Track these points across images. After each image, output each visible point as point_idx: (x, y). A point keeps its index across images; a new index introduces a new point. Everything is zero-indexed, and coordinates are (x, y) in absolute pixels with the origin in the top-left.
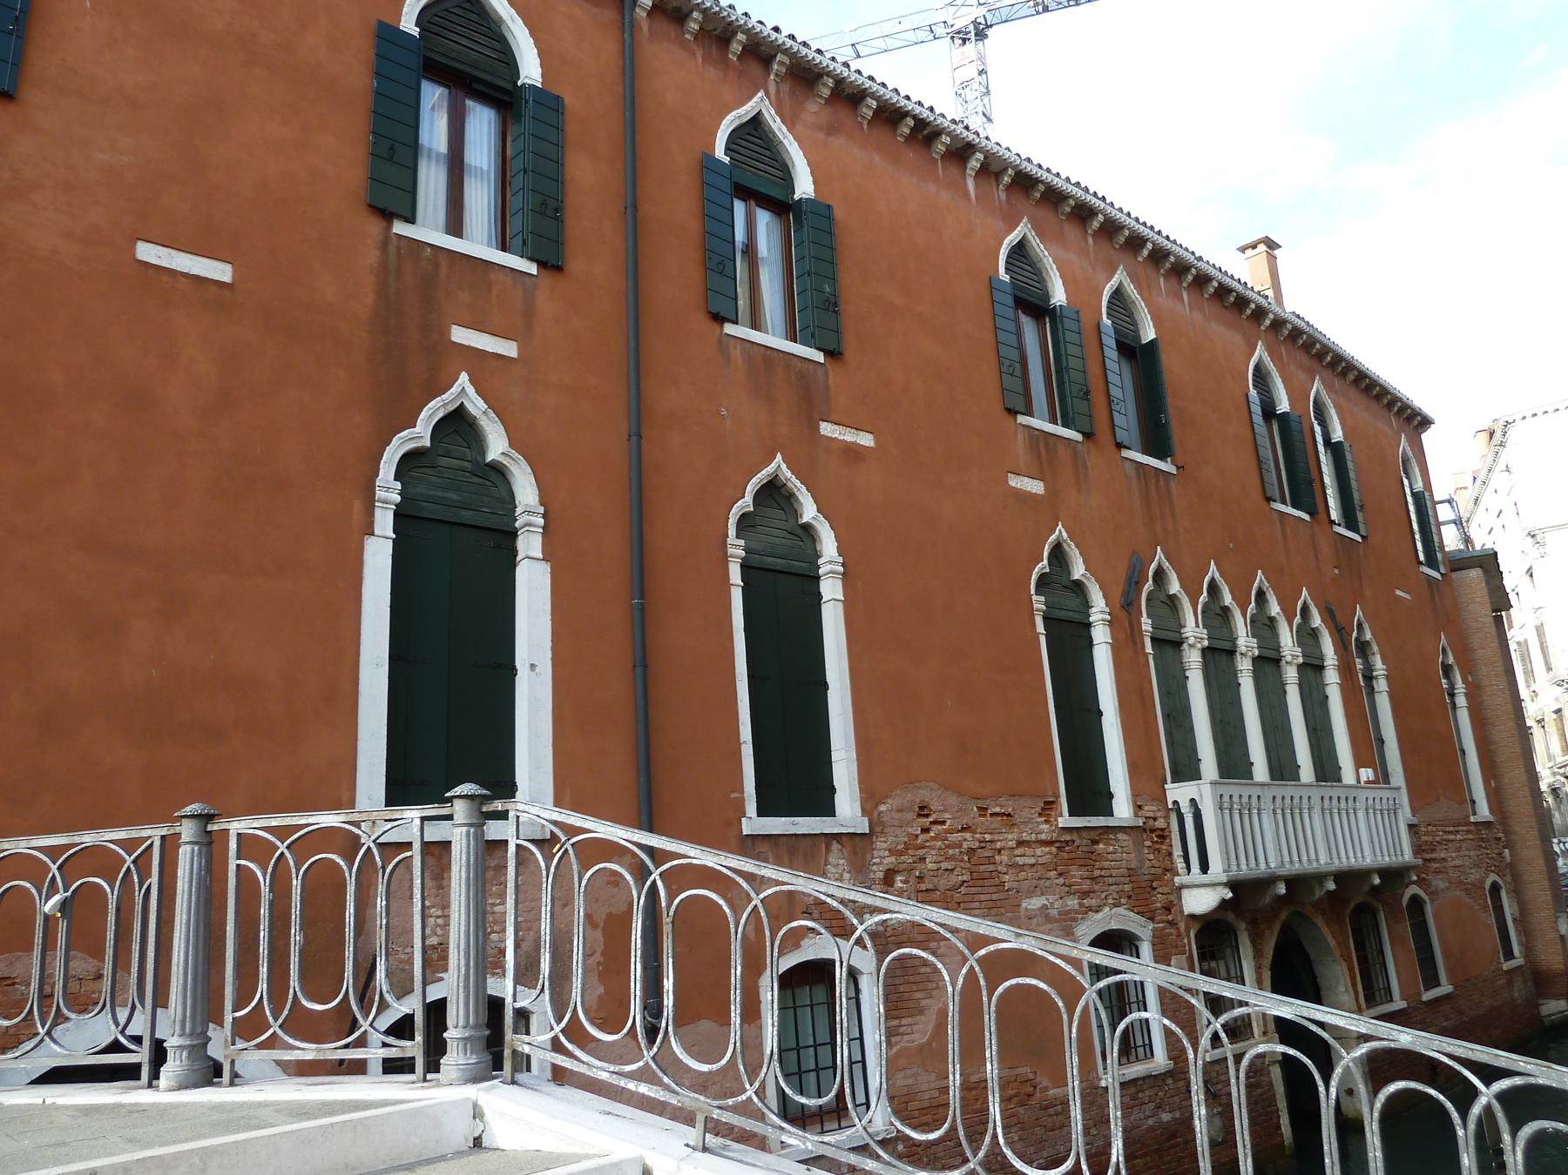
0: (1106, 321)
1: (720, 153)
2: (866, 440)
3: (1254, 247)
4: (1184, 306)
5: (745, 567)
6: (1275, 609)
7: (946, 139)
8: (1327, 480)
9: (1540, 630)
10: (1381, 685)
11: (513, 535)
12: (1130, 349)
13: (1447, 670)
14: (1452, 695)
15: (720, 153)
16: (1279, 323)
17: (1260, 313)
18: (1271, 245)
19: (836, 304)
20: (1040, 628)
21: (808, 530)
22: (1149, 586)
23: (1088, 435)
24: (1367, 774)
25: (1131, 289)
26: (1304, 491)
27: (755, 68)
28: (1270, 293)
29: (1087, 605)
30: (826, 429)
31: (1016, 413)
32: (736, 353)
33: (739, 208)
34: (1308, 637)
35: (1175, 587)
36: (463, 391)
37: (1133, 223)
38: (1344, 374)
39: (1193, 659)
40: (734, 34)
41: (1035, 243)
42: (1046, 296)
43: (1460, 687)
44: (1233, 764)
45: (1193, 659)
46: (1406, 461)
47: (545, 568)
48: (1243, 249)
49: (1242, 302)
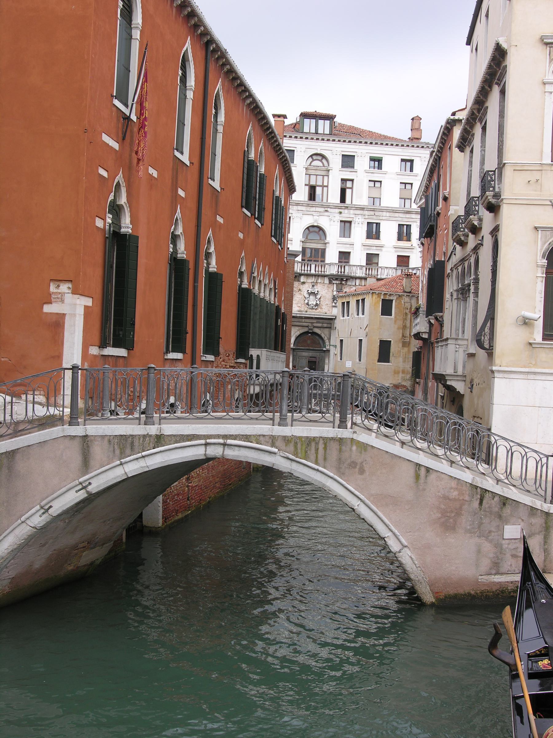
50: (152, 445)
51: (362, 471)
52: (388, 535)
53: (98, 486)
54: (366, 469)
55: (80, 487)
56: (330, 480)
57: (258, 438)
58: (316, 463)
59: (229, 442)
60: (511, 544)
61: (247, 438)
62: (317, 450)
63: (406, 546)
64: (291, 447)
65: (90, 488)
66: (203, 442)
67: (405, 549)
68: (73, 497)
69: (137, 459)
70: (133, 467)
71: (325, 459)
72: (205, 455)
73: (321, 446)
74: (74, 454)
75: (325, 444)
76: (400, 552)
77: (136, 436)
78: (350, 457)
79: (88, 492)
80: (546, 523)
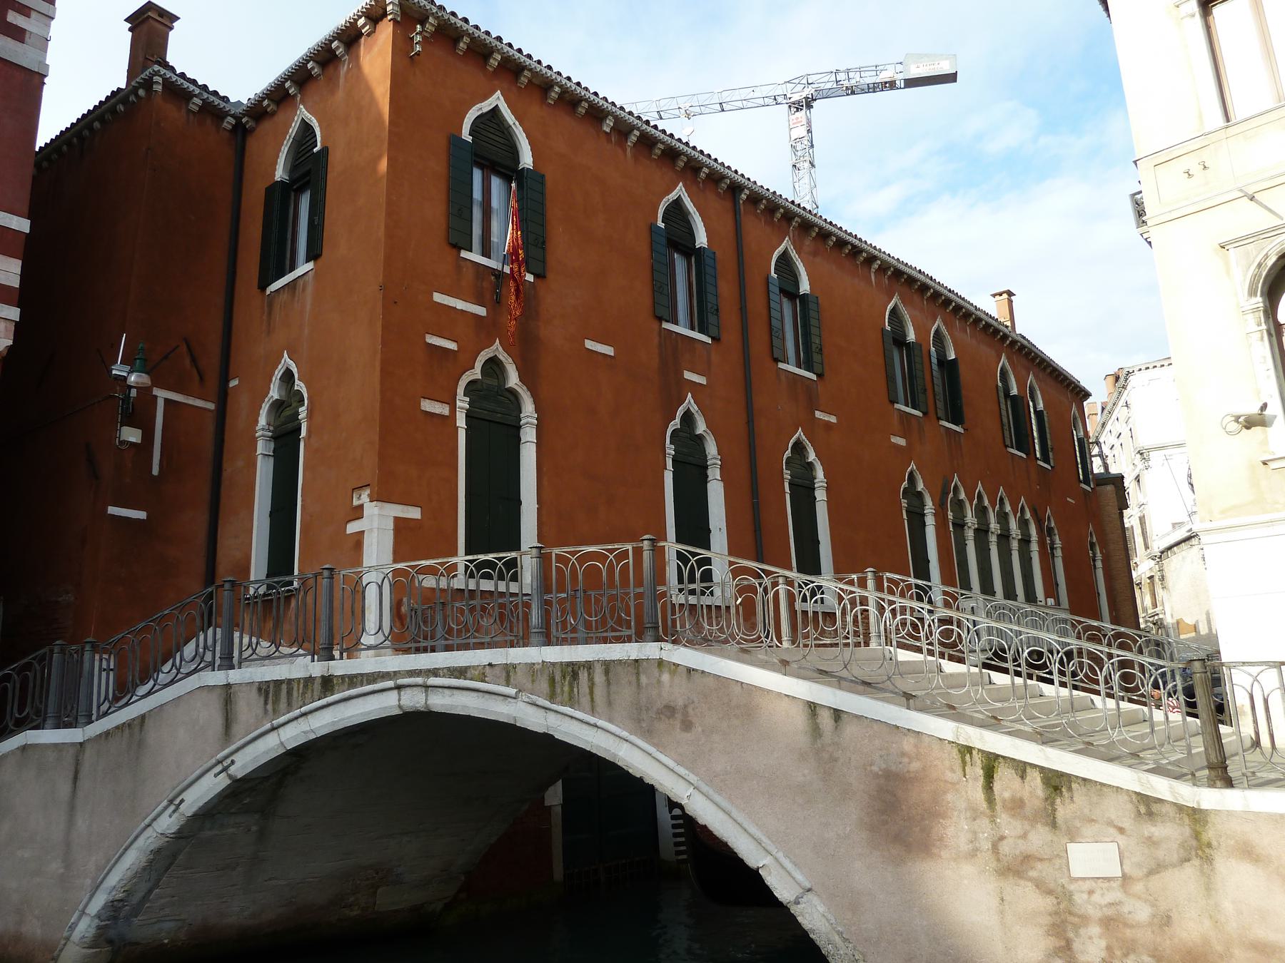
0: (933, 349)
1: (466, 135)
2: (833, 419)
3: (1001, 294)
4: (967, 337)
5: (469, 416)
6: (1008, 508)
7: (864, 255)
8: (1035, 434)
9: (1142, 520)
10: (1059, 553)
11: (519, 428)
12: (943, 362)
13: (1092, 545)
14: (1094, 561)
15: (466, 135)
16: (1014, 342)
17: (1005, 337)
18: (1010, 294)
19: (544, 243)
20: (787, 490)
21: (811, 465)
22: (951, 495)
23: (925, 414)
24: (1051, 601)
25: (943, 328)
26: (1023, 442)
27: (784, 224)
28: (1008, 324)
29: (923, 505)
30: (818, 414)
31: (460, 248)
32: (783, 378)
33: (477, 175)
34: (1023, 524)
35: (962, 496)
36: (690, 402)
37: (712, 163)
38: (1045, 369)
39: (970, 534)
40: (552, 86)
41: (901, 306)
42: (905, 336)
43: (1099, 555)
44: (987, 589)
45: (970, 534)
46: (1075, 419)
47: (721, 484)
48: (994, 296)
49: (997, 331)
50: (316, 694)
51: (687, 726)
52: (764, 862)
53: (244, 767)
54: (694, 720)
55: (219, 768)
56: (626, 745)
57: (482, 673)
58: (593, 711)
59: (433, 681)
60: (1099, 892)
61: (461, 672)
62: (591, 679)
63: (809, 890)
64: (544, 685)
65: (232, 770)
66: (390, 684)
67: (810, 896)
68: (210, 787)
69: (296, 718)
70: (293, 734)
71: (610, 703)
72: (400, 706)
73: (599, 678)
74: (211, 714)
75: (607, 672)
76: (797, 902)
77: (281, 682)
78: (660, 695)
79: (230, 776)
80: (1197, 835)
